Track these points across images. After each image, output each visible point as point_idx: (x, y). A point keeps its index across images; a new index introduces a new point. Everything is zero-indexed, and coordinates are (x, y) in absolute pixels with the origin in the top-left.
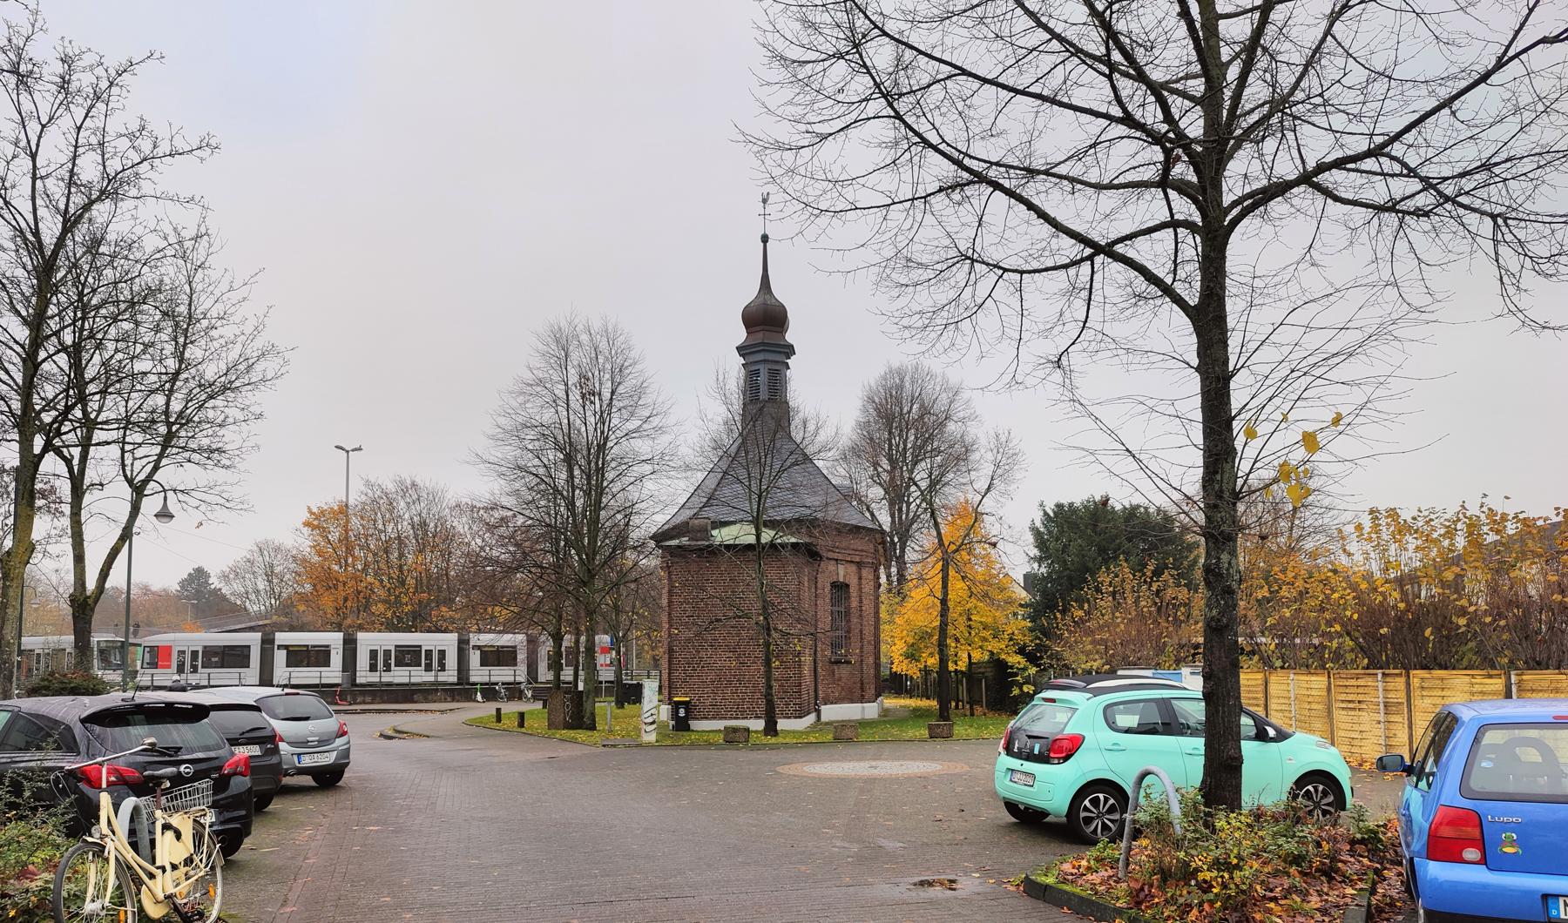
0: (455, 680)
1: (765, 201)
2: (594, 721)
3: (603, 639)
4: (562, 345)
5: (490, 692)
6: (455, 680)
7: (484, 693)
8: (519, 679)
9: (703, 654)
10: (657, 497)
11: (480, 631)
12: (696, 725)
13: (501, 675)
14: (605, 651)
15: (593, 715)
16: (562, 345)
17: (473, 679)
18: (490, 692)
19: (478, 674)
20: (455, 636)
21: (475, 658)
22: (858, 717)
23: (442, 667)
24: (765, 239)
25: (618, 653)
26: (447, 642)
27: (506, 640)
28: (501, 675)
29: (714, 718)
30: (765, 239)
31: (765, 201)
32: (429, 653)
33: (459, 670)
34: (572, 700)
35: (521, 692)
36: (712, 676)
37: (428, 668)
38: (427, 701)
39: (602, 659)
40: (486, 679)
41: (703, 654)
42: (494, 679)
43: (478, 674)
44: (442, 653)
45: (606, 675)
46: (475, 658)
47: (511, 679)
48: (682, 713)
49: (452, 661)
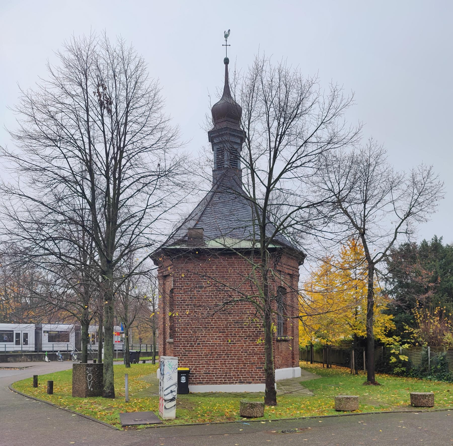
0: (34, 349)
1: (226, 36)
2: (113, 389)
3: (117, 328)
4: (82, 67)
5: (53, 356)
6: (34, 349)
7: (49, 356)
8: (69, 349)
9: (198, 334)
10: (162, 214)
11: (49, 323)
12: (193, 388)
13: (60, 347)
14: (119, 334)
15: (112, 384)
16: (82, 67)
17: (44, 349)
18: (53, 356)
19: (47, 346)
20: (33, 325)
21: (45, 338)
22: (290, 377)
23: (26, 342)
24: (226, 61)
25: (127, 334)
26: (30, 329)
27: (63, 327)
28: (60, 347)
29: (207, 383)
30: (226, 61)
31: (226, 36)
32: (18, 335)
33: (36, 344)
34: (93, 372)
35: (71, 356)
36: (206, 351)
37: (18, 343)
38: (16, 361)
39: (116, 338)
40: (51, 349)
41: (198, 334)
42: (55, 349)
43: (47, 346)
44: (26, 335)
45: (118, 346)
46: (45, 338)
47: (65, 349)
48: (183, 380)
49: (31, 339)
